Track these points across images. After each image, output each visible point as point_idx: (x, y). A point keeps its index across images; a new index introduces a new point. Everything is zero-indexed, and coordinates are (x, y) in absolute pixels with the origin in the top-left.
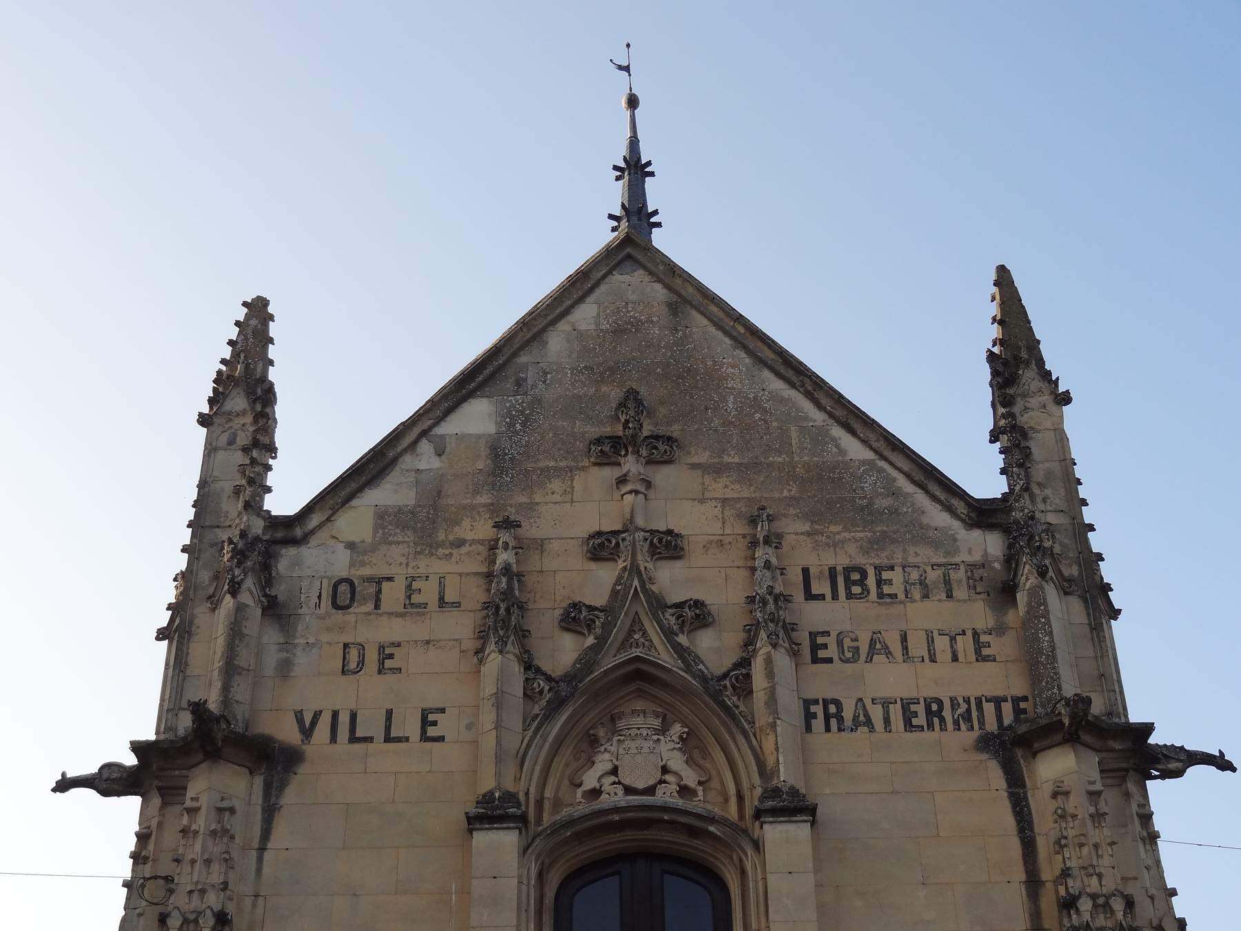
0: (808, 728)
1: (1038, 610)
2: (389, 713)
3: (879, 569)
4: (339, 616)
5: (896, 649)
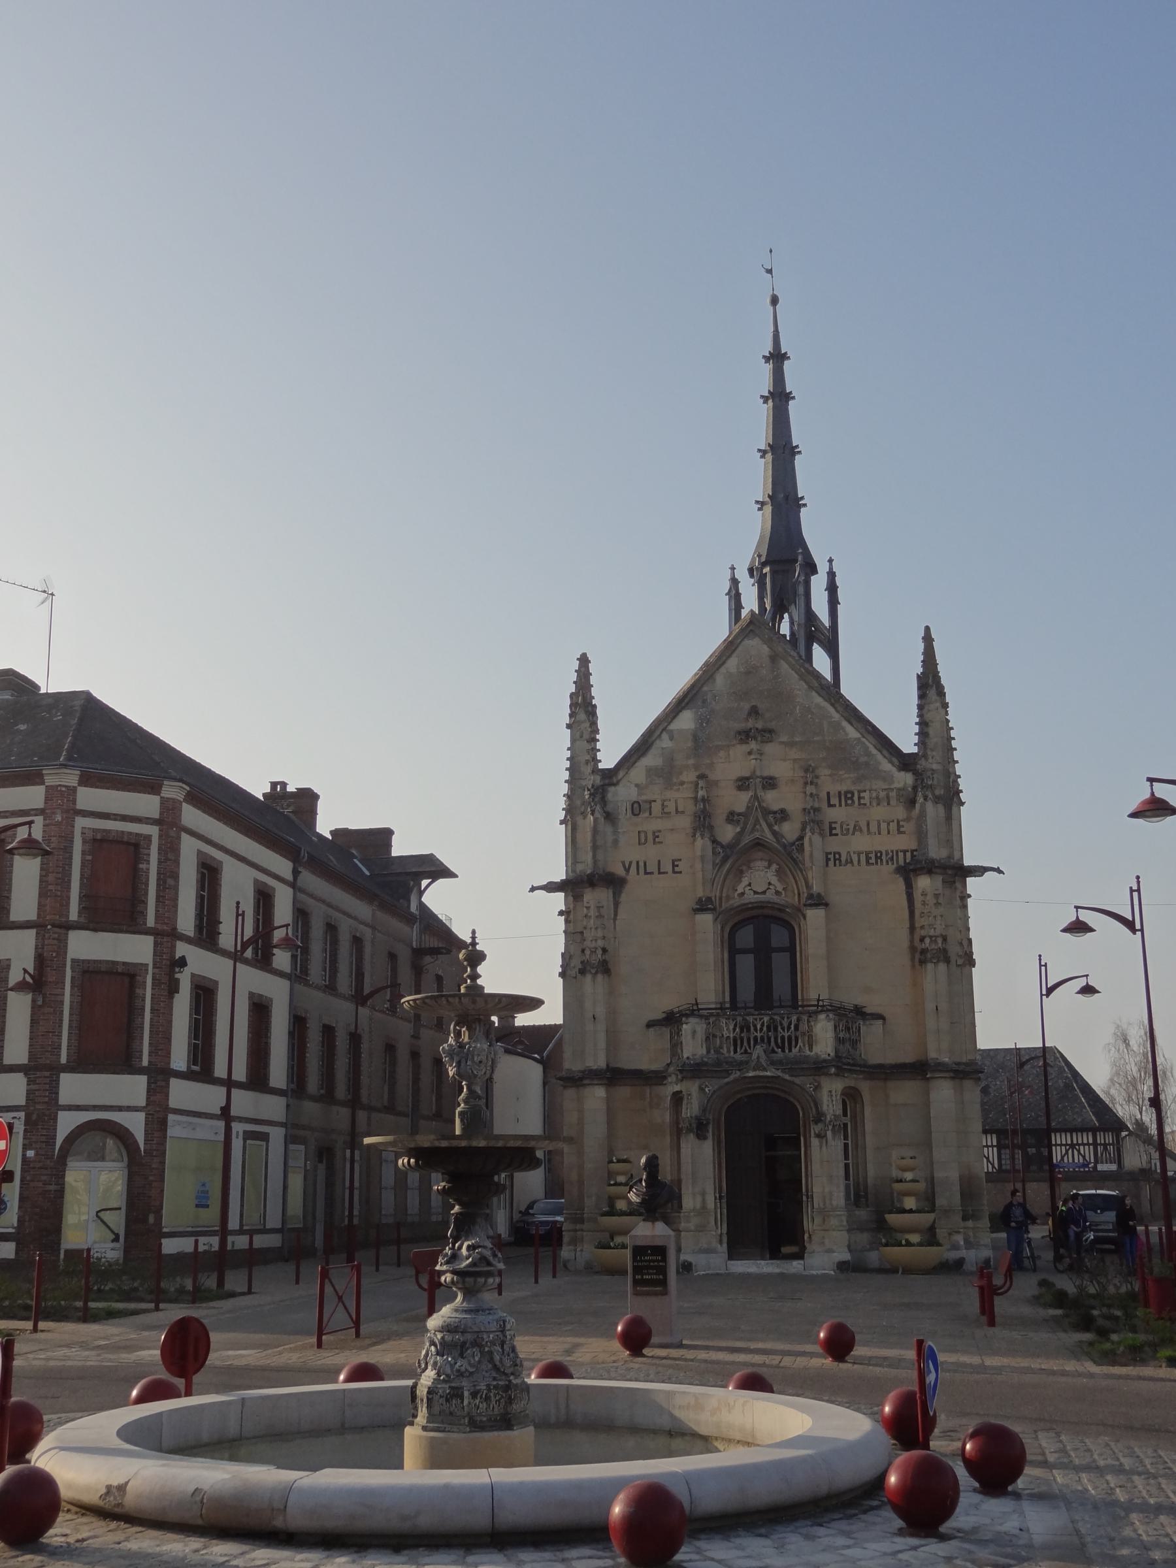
0: (827, 865)
1: (923, 814)
2: (659, 861)
3: (859, 792)
4: (635, 819)
5: (865, 829)
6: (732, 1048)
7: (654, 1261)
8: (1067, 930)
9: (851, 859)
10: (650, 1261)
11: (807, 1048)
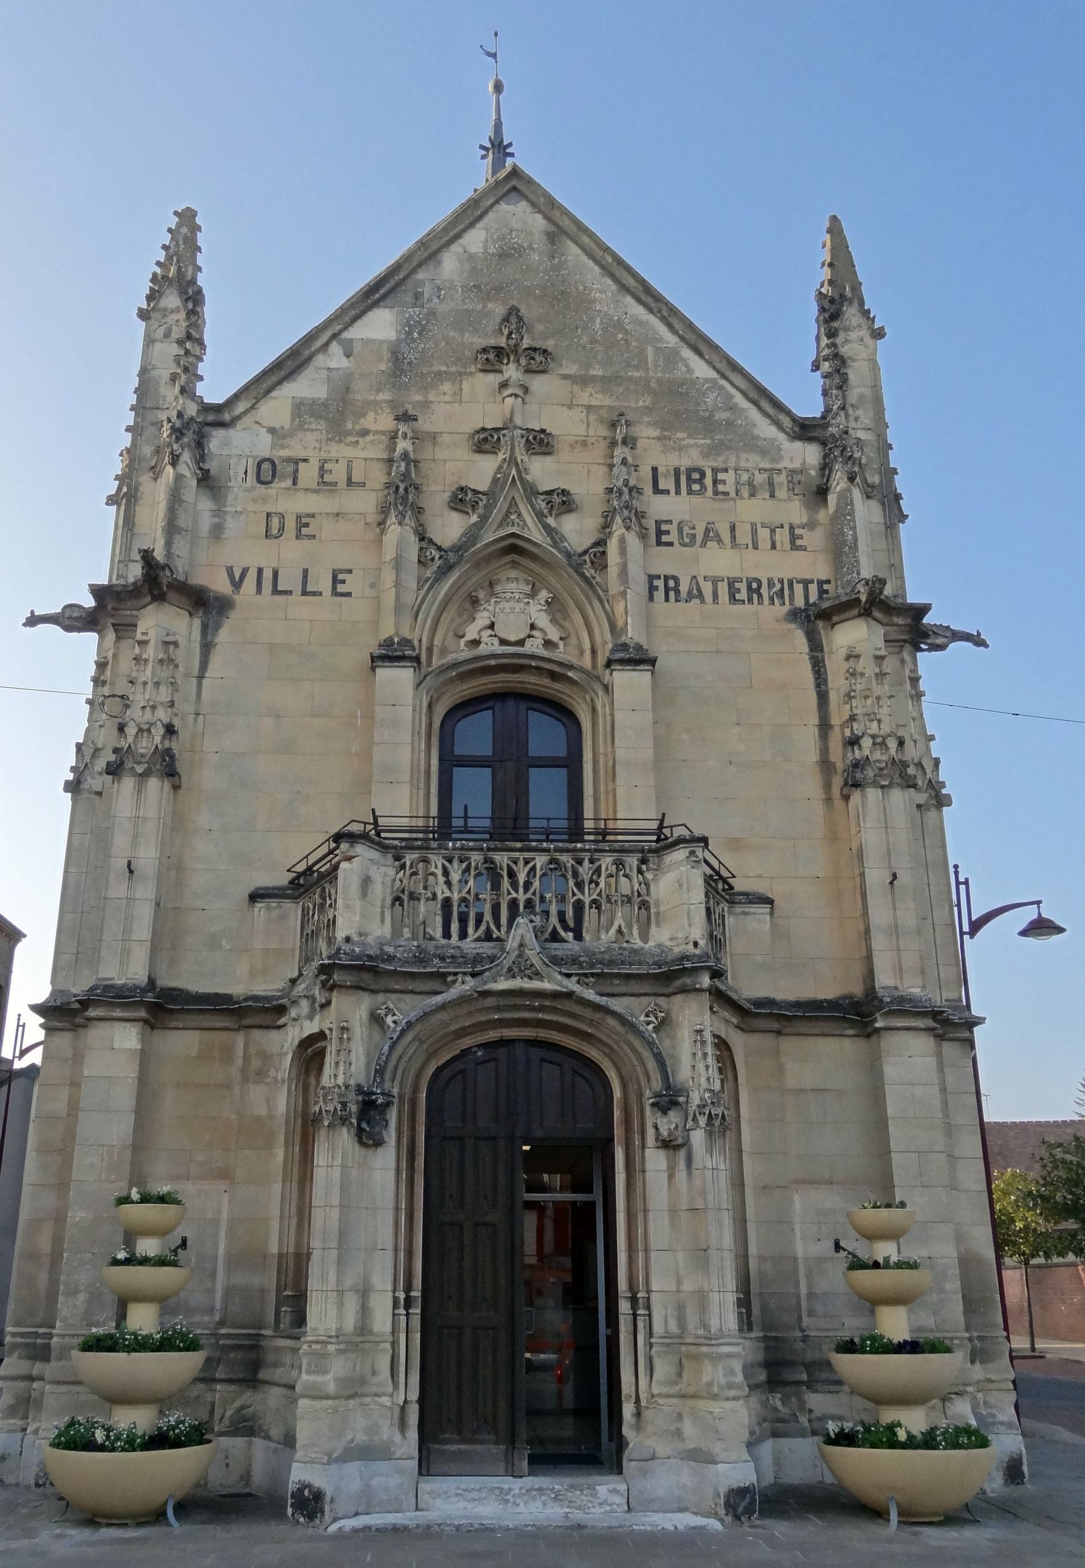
0: (651, 598)
2: (306, 572)
3: (715, 471)
5: (726, 537)
6: (455, 927)
9: (699, 590)
11: (635, 932)
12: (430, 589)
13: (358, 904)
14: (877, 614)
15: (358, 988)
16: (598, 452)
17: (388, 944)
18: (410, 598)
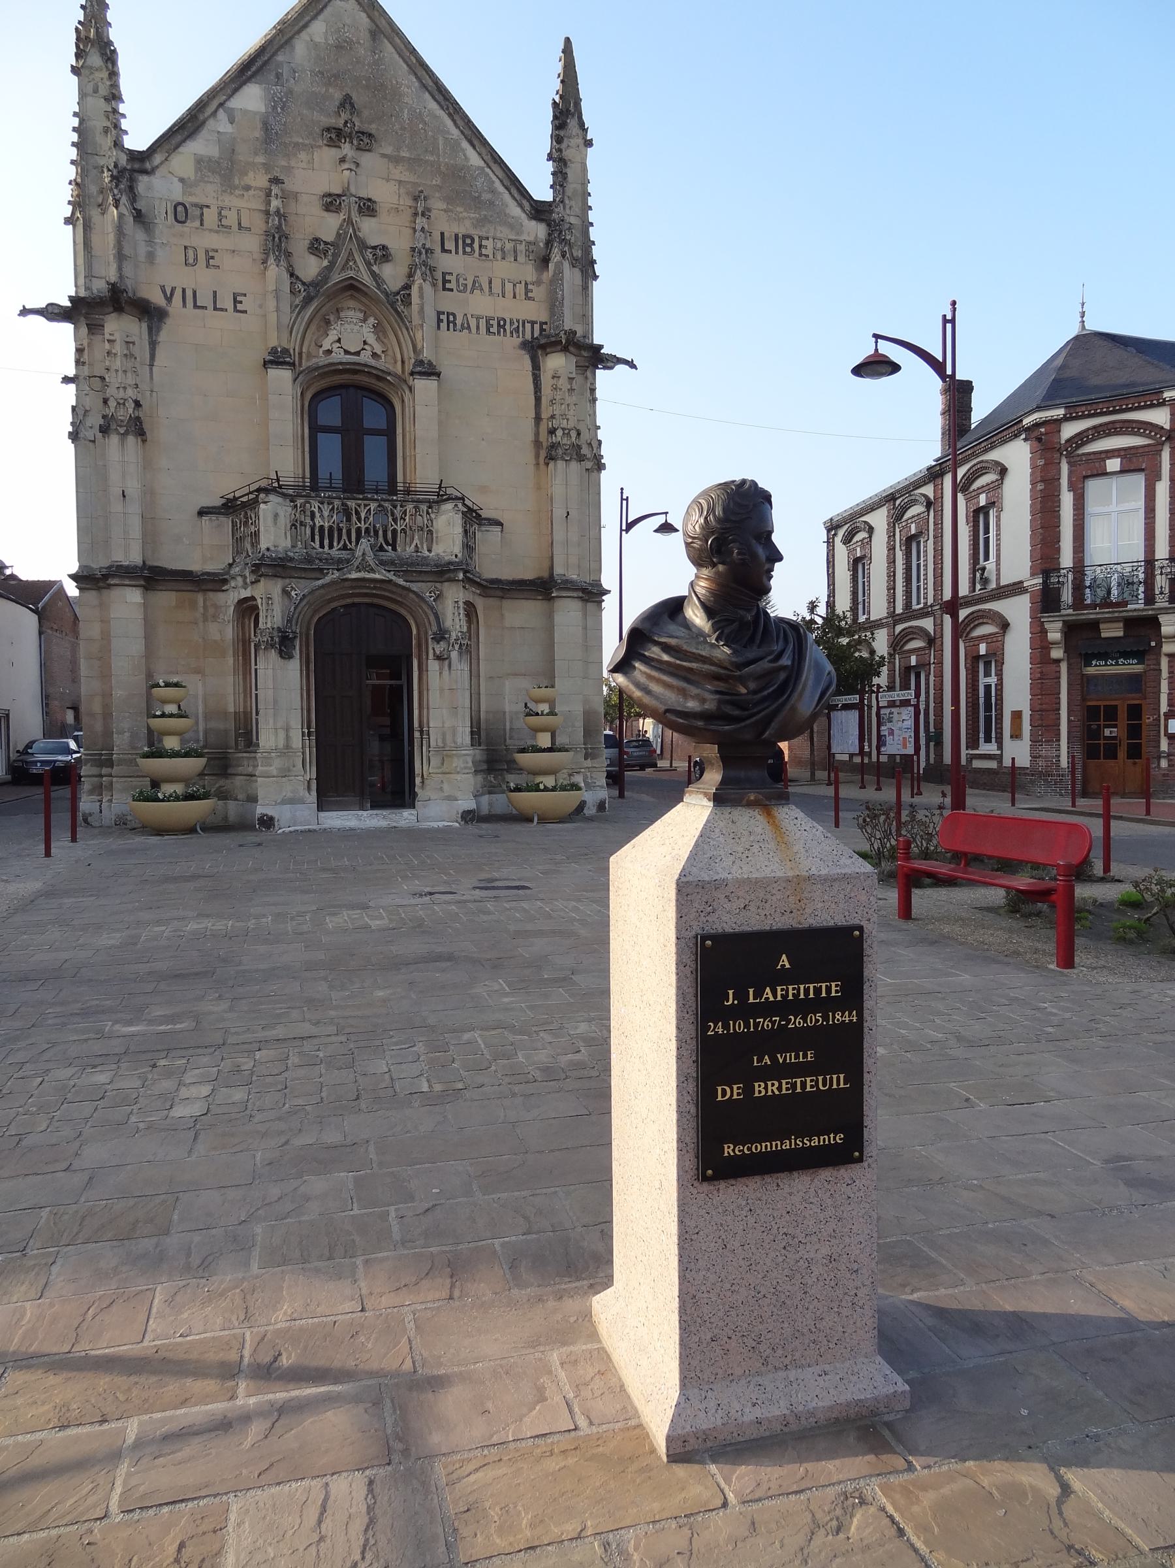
0: (439, 328)
1: (558, 278)
2: (215, 293)
3: (481, 238)
5: (486, 287)
6: (326, 542)
7: (802, 1007)
8: (858, 371)
9: (468, 324)
10: (784, 1008)
11: (425, 547)
12: (299, 313)
13: (272, 529)
14: (571, 349)
15: (276, 576)
16: (407, 216)
17: (290, 551)
18: (286, 319)
